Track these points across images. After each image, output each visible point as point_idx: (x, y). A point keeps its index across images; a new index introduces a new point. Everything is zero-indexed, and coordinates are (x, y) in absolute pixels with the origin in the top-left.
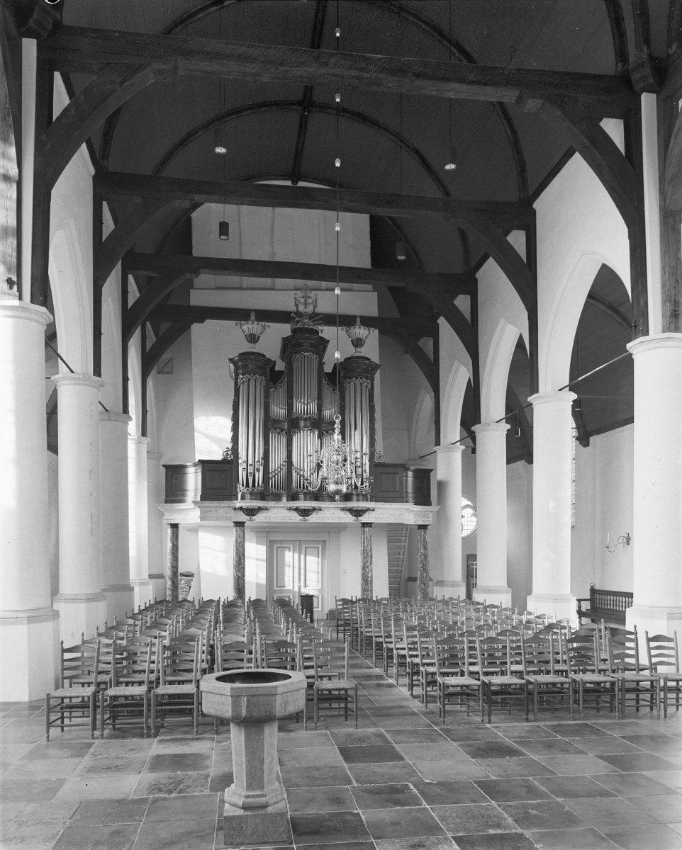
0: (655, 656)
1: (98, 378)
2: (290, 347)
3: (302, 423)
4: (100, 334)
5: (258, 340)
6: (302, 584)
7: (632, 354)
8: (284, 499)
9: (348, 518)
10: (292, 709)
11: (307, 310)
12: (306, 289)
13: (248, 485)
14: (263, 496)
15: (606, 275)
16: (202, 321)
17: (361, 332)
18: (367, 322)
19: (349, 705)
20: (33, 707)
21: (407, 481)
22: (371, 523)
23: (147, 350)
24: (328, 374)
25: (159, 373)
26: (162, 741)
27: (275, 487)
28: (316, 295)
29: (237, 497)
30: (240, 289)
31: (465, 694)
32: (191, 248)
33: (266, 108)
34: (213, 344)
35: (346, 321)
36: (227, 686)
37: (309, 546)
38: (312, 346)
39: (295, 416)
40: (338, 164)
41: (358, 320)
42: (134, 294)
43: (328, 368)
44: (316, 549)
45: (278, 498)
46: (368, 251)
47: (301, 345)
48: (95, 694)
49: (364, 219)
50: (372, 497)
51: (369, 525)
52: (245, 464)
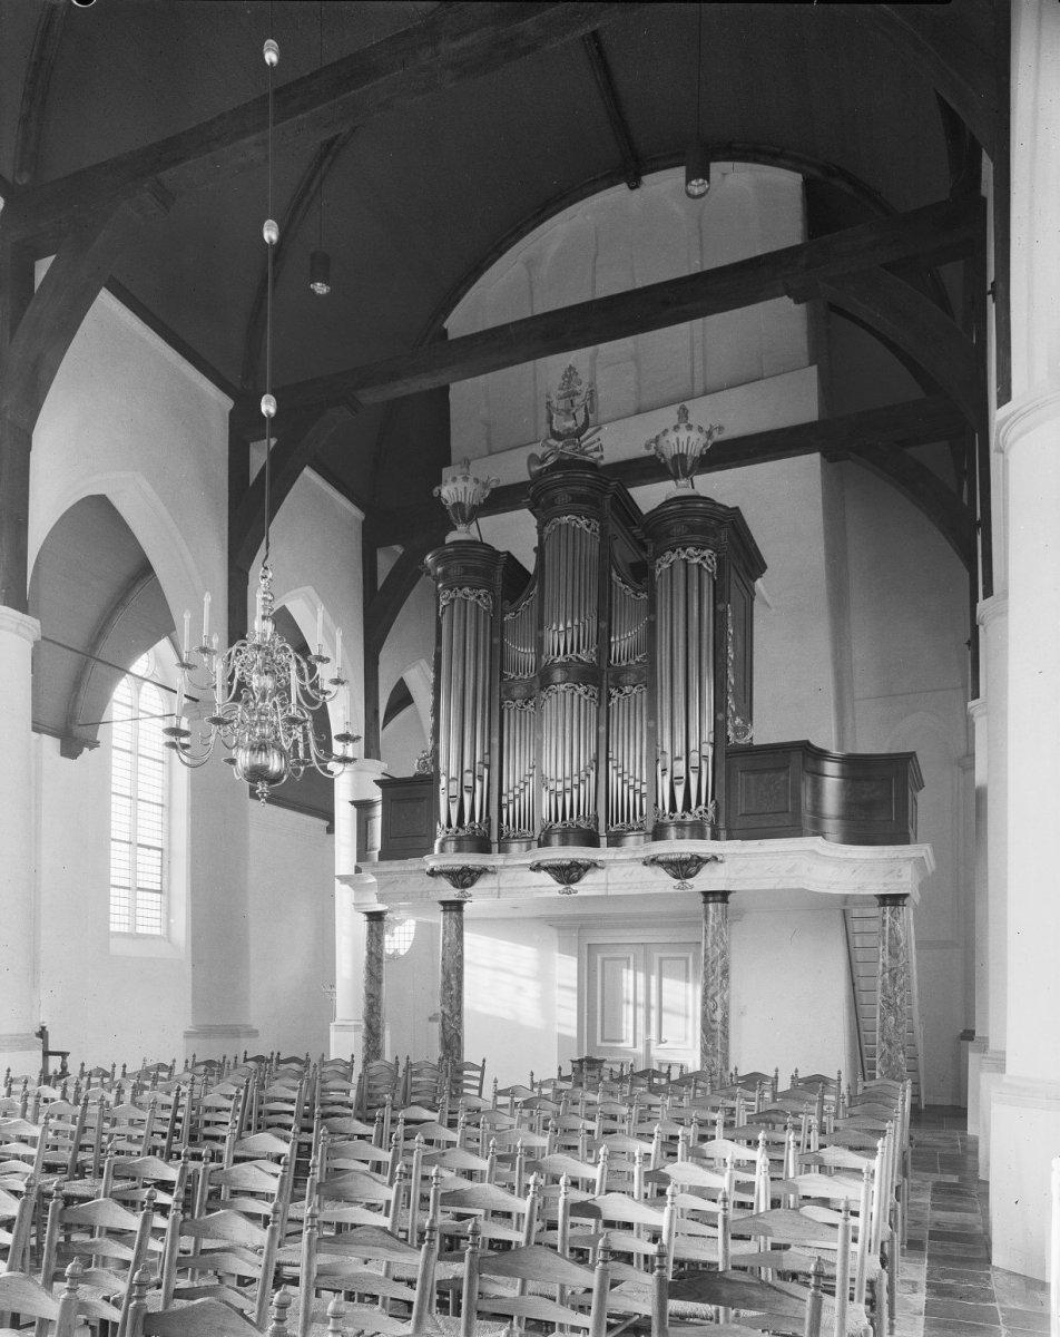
3: (558, 675)
6: (654, 1035)
13: (449, 825)
23: (380, 583)
27: (514, 826)
37: (667, 955)
38: (578, 499)
40: (271, 57)
51: (723, 896)
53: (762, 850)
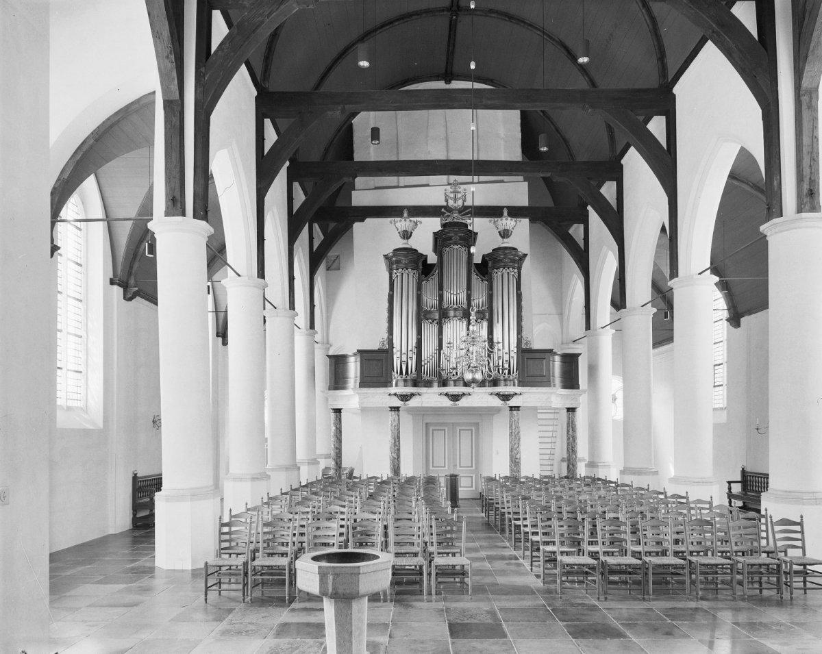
0: (797, 540)
1: (261, 280)
2: (440, 240)
3: (452, 313)
4: (263, 240)
5: (411, 235)
7: (766, 236)
8: (436, 384)
9: (497, 402)
10: (376, 588)
11: (456, 205)
12: (456, 184)
13: (401, 373)
14: (415, 383)
15: (744, 155)
16: (363, 220)
17: (507, 222)
18: (515, 212)
19: (466, 580)
20: (195, 573)
21: (553, 366)
22: (519, 407)
24: (476, 265)
25: (327, 270)
26: (293, 610)
28: (465, 190)
29: (392, 384)
30: (397, 187)
31: (583, 572)
32: (352, 152)
33: (416, 17)
34: (373, 241)
35: (492, 212)
36: (316, 565)
39: (445, 306)
41: (505, 212)
42: (300, 197)
43: (478, 260)
44: (470, 432)
45: (428, 384)
46: (519, 142)
47: (450, 238)
48: (245, 564)
49: (515, 115)
50: (519, 382)
51: (517, 408)
52: (399, 353)
53: (537, 391)
